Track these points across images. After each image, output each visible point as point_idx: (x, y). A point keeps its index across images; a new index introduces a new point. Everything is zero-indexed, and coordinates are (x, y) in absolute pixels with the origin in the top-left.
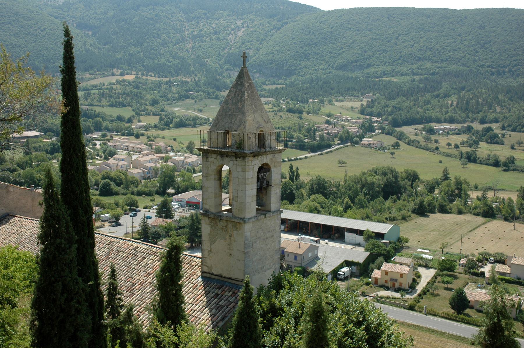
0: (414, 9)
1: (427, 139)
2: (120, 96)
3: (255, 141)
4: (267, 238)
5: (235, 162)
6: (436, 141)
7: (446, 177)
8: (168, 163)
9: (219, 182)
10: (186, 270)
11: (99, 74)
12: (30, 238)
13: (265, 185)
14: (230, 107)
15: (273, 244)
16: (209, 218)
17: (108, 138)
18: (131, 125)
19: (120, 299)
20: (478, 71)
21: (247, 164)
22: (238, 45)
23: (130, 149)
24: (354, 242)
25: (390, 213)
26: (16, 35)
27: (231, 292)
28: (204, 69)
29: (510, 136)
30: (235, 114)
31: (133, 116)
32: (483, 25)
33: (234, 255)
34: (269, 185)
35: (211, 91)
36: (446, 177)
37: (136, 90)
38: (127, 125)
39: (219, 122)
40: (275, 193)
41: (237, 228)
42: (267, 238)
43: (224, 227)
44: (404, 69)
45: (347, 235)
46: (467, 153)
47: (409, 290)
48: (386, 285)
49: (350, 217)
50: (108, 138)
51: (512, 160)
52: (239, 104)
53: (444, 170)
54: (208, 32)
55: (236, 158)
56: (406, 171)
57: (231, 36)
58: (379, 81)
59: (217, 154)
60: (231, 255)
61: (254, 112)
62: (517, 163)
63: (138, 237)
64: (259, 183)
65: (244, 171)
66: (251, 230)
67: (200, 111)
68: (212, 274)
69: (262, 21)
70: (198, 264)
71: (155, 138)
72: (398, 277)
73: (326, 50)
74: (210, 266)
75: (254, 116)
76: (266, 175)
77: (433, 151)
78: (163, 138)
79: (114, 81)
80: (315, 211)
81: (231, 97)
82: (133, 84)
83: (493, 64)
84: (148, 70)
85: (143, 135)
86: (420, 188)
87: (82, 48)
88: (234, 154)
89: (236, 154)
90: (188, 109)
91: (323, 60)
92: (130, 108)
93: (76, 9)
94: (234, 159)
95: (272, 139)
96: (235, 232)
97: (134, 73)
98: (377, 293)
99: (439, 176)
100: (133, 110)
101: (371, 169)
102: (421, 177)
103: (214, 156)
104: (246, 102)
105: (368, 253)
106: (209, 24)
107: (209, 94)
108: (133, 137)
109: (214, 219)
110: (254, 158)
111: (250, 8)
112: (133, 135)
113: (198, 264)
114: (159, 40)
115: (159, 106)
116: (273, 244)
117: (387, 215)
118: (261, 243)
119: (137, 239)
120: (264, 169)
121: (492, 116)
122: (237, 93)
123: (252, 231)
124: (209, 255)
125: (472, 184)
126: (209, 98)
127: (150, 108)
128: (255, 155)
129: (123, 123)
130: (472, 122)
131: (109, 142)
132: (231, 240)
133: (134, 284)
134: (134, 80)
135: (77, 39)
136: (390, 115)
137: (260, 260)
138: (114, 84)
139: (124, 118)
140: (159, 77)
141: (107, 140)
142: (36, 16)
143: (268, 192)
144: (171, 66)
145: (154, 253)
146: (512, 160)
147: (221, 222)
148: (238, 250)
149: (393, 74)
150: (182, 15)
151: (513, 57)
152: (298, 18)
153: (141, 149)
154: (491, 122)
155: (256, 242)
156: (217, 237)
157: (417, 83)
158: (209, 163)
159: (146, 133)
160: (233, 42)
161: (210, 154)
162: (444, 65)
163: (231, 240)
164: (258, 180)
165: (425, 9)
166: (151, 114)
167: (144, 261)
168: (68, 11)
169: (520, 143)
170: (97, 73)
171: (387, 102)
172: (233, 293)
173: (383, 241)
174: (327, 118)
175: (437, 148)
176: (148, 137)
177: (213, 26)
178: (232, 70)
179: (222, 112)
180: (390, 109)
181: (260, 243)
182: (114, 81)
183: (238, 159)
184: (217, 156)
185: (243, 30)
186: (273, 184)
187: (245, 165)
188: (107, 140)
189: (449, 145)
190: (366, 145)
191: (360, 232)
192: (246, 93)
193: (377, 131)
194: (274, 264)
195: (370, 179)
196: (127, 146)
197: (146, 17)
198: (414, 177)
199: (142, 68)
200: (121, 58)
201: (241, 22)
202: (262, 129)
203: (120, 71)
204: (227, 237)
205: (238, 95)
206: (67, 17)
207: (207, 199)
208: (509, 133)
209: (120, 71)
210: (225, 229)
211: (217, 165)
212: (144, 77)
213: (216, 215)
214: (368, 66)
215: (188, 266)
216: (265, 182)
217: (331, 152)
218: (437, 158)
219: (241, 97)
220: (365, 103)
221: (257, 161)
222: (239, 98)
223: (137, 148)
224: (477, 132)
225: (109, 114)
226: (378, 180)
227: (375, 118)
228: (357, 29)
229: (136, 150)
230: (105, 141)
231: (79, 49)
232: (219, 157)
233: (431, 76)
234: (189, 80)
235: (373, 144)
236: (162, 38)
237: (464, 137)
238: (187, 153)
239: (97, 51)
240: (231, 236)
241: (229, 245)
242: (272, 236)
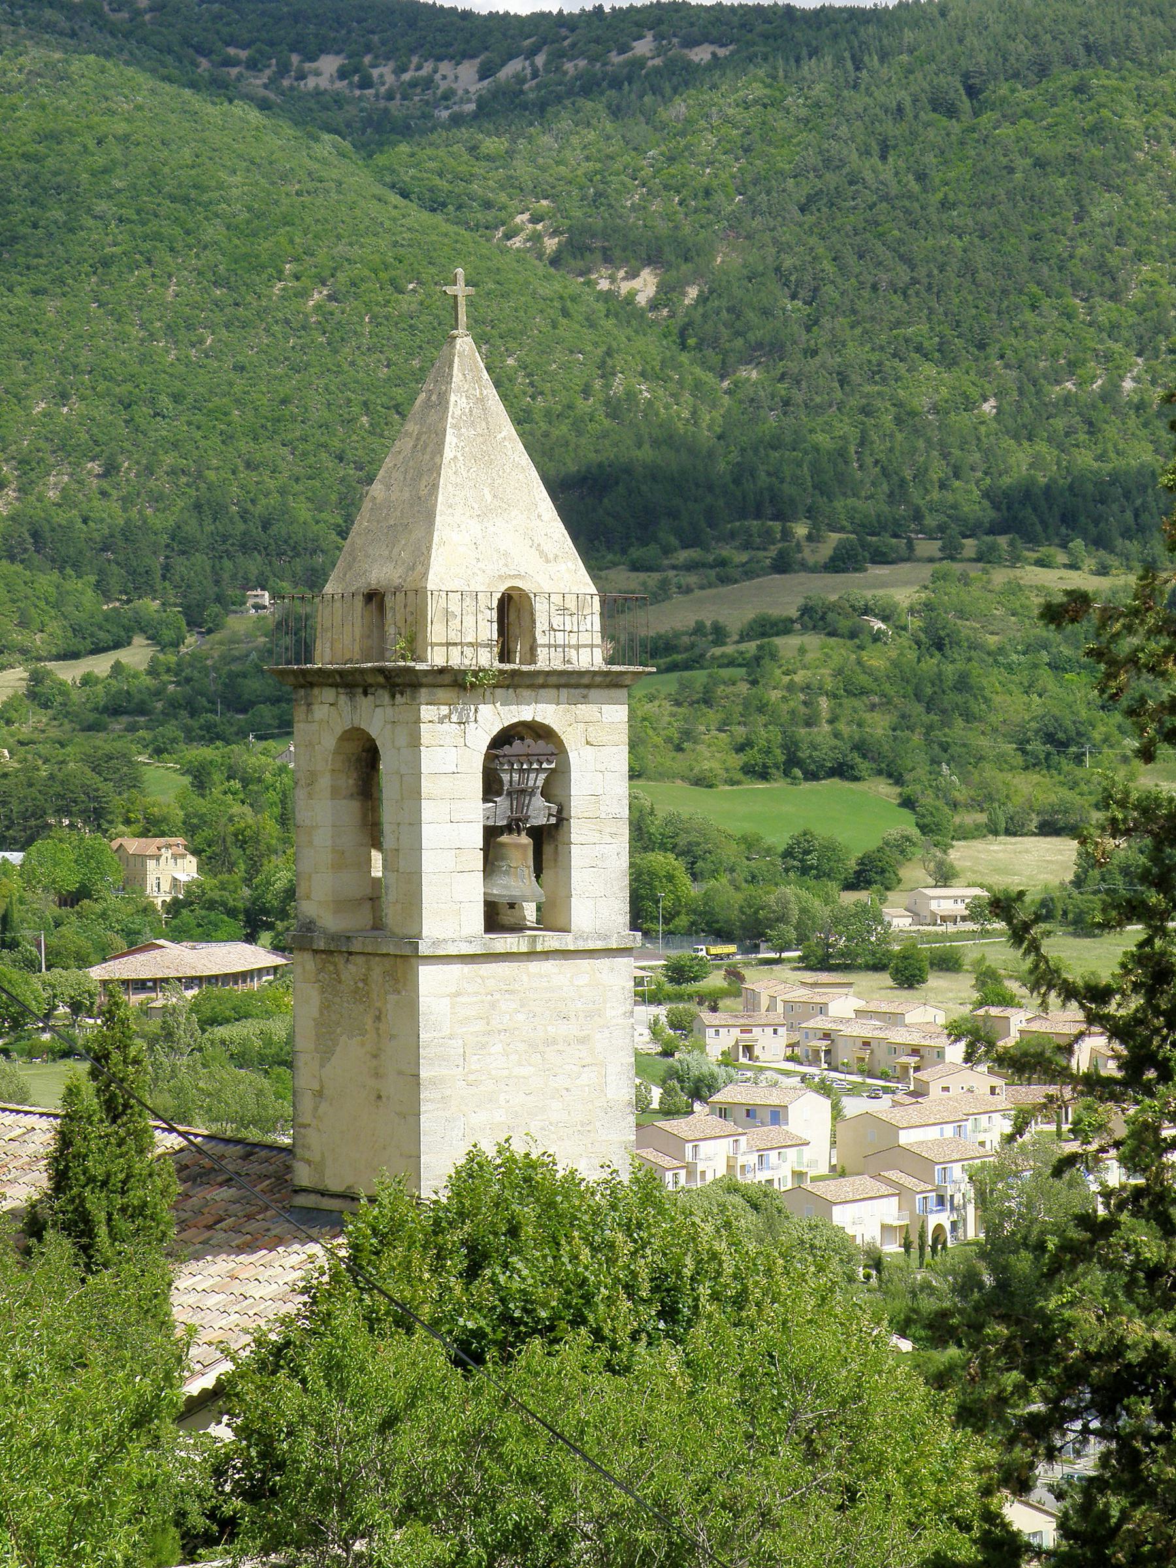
2: (824, 703)
5: (389, 711)
9: (354, 806)
11: (691, 567)
16: (316, 952)
17: (716, 980)
18: (883, 900)
23: (844, 1056)
26: (182, 334)
31: (902, 846)
37: (931, 663)
41: (397, 981)
43: (361, 985)
50: (716, 980)
55: (393, 697)
60: (379, 1097)
68: (323, 1194)
74: (317, 1158)
79: (794, 613)
81: (401, 457)
85: (947, 963)
88: (381, 679)
92: (884, 789)
94: (386, 697)
96: (392, 998)
103: (329, 694)
108: (885, 979)
109: (331, 952)
114: (1105, 310)
122: (424, 437)
123: (458, 994)
129: (833, 886)
131: (714, 1009)
138: (787, 631)
139: (831, 850)
141: (701, 999)
142: (306, 199)
143: (560, 847)
147: (350, 966)
153: (915, 1051)
156: (339, 1030)
158: (315, 726)
159: (971, 951)
161: (316, 691)
166: (1033, 826)
170: (683, 556)
182: (794, 613)
188: (701, 999)
192: (450, 438)
196: (826, 1036)
200: (842, 453)
204: (369, 1021)
205: (425, 446)
222: (427, 457)
223: (894, 1049)
225: (737, 828)
229: (884, 1062)
230: (692, 1007)
231: (570, 407)
232: (343, 699)
236: (1134, 294)
239: (686, 414)
240: (378, 1018)
241: (375, 1056)
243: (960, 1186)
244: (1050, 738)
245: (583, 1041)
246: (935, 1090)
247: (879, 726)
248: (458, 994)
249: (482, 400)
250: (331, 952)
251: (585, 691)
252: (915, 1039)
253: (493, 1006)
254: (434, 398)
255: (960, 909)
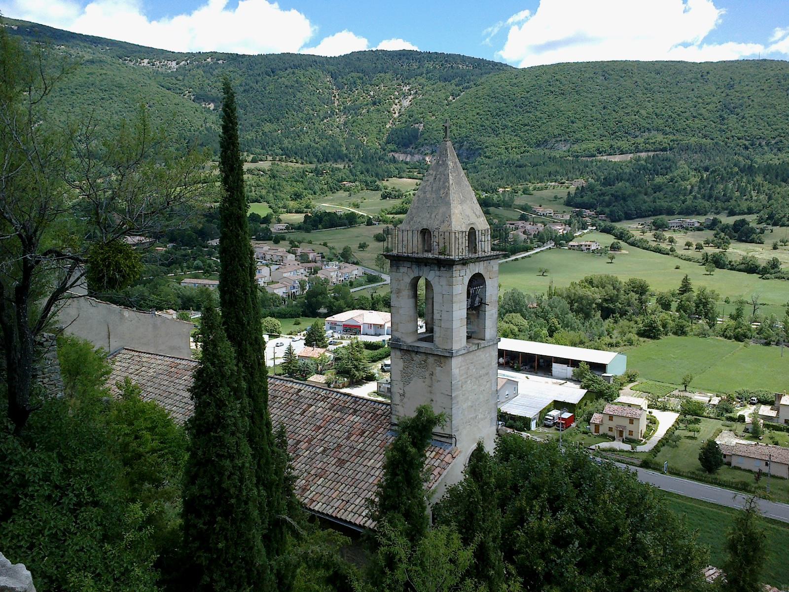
0: (638, 62)
1: (657, 237)
3: (464, 242)
4: (480, 377)
5: (438, 273)
6: (671, 241)
7: (686, 288)
8: (318, 275)
10: (369, 421)
12: (154, 380)
13: (477, 304)
14: (428, 196)
15: (488, 385)
19: (290, 467)
20: (726, 144)
21: (454, 275)
22: (404, 117)
24: (564, 376)
25: (611, 337)
27: (434, 453)
28: (361, 152)
29: (772, 232)
30: (435, 205)
32: (732, 83)
33: (436, 401)
34: (482, 303)
35: (369, 179)
36: (686, 288)
37: (273, 181)
38: (264, 226)
39: (413, 217)
40: (491, 312)
42: (480, 377)
44: (623, 144)
45: (556, 367)
46: (714, 256)
47: (642, 441)
48: (610, 433)
49: (558, 343)
51: (774, 264)
52: (442, 192)
53: (684, 279)
54: (365, 103)
56: (632, 282)
57: (394, 106)
58: (592, 162)
59: (411, 262)
61: (462, 203)
62: (782, 267)
63: (281, 371)
64: (470, 300)
65: (451, 285)
66: (459, 366)
67: (357, 206)
69: (435, 86)
70: (384, 413)
71: (300, 242)
72: (626, 422)
73: (521, 122)
75: (462, 208)
76: (479, 289)
77: (668, 254)
78: (310, 242)
80: (511, 335)
82: (269, 173)
83: (746, 134)
84: (288, 154)
85: (284, 239)
86: (652, 304)
87: (202, 126)
88: (436, 262)
89: (438, 262)
90: (341, 205)
91: (516, 135)
93: (194, 76)
95: (486, 240)
97: (270, 158)
98: (599, 444)
99: (677, 285)
100: (270, 207)
101: (583, 279)
102: (652, 288)
103: (409, 264)
104: (451, 188)
105: (586, 391)
106: (366, 92)
107: (367, 185)
108: (272, 242)
110: (465, 267)
111: (419, 68)
112: (271, 240)
113: (384, 413)
114: (300, 115)
115: (304, 201)
116: (488, 385)
117: (607, 339)
118: (473, 384)
119: (280, 375)
120: (477, 281)
121: (744, 205)
122: (438, 176)
123: (460, 367)
124: (402, 400)
125: (723, 296)
126: (367, 189)
127: (292, 204)
128: (464, 262)
130: (718, 213)
132: (432, 380)
133: (299, 442)
134: (270, 168)
135: (196, 116)
136: (608, 206)
137: (472, 407)
139: (258, 216)
140: (302, 163)
144: (318, 149)
145: (324, 399)
146: (774, 264)
148: (442, 393)
149: (613, 151)
150: (330, 80)
151: (773, 125)
152: (483, 79)
154: (744, 213)
155: (466, 382)
157: (643, 162)
158: (400, 274)
160: (397, 115)
161: (401, 262)
162: (678, 136)
163: (432, 380)
164: (468, 297)
165: (653, 63)
166: (294, 211)
167: (310, 409)
168: (183, 79)
169: (784, 242)
171: (603, 189)
172: (437, 453)
173: (604, 375)
174: (523, 212)
175: (672, 250)
176: (291, 242)
177: (372, 93)
178: (397, 152)
179: (418, 203)
180: (607, 198)
181: (471, 383)
183: (442, 269)
184: (412, 264)
185: (410, 97)
186: (487, 301)
187: (452, 277)
189: (688, 244)
190: (576, 247)
191: (574, 363)
192: (450, 177)
193: (590, 228)
194: (489, 413)
195: (581, 292)
197: (283, 84)
198: (641, 289)
199: (280, 152)
201: (408, 87)
202: (473, 226)
203: (252, 156)
204: (427, 374)
205: (440, 179)
206: (183, 88)
207: (398, 324)
208: (770, 227)
209: (252, 156)
210: (424, 365)
211: (412, 276)
212: (284, 164)
213: (411, 346)
214: (577, 141)
215: (372, 416)
216: (477, 299)
217: (529, 256)
218: (672, 261)
219: (444, 183)
220: (572, 189)
221: (468, 271)
224: (727, 226)
226: (596, 295)
227: (586, 211)
228: (562, 92)
232: (414, 266)
233: (662, 153)
234: (341, 166)
235: (586, 245)
237: (709, 234)
238: (341, 261)
240: (432, 375)
242: (487, 374)
243: (297, 284)
244: (295, 195)
245: (487, 374)
246: (287, 265)
247: (264, 192)
248: (460, 367)
249: (456, 163)
250: (409, 350)
251: (489, 261)
252: (281, 254)
253: (468, 368)
254: (440, 162)
255: (284, 228)
